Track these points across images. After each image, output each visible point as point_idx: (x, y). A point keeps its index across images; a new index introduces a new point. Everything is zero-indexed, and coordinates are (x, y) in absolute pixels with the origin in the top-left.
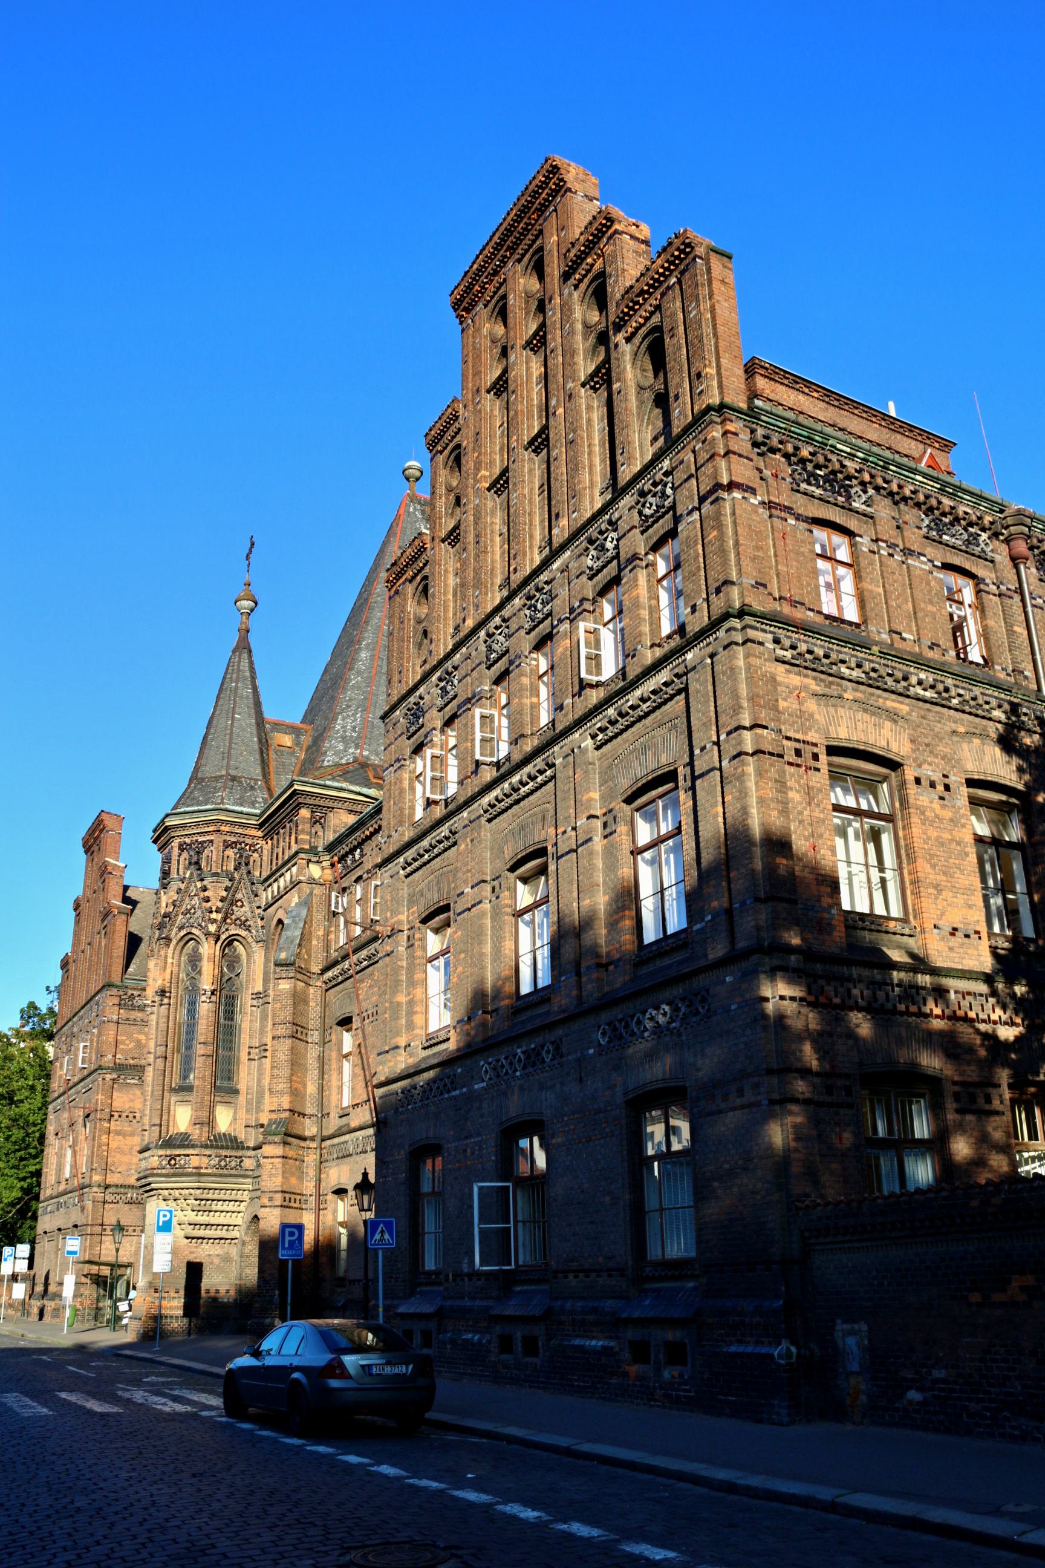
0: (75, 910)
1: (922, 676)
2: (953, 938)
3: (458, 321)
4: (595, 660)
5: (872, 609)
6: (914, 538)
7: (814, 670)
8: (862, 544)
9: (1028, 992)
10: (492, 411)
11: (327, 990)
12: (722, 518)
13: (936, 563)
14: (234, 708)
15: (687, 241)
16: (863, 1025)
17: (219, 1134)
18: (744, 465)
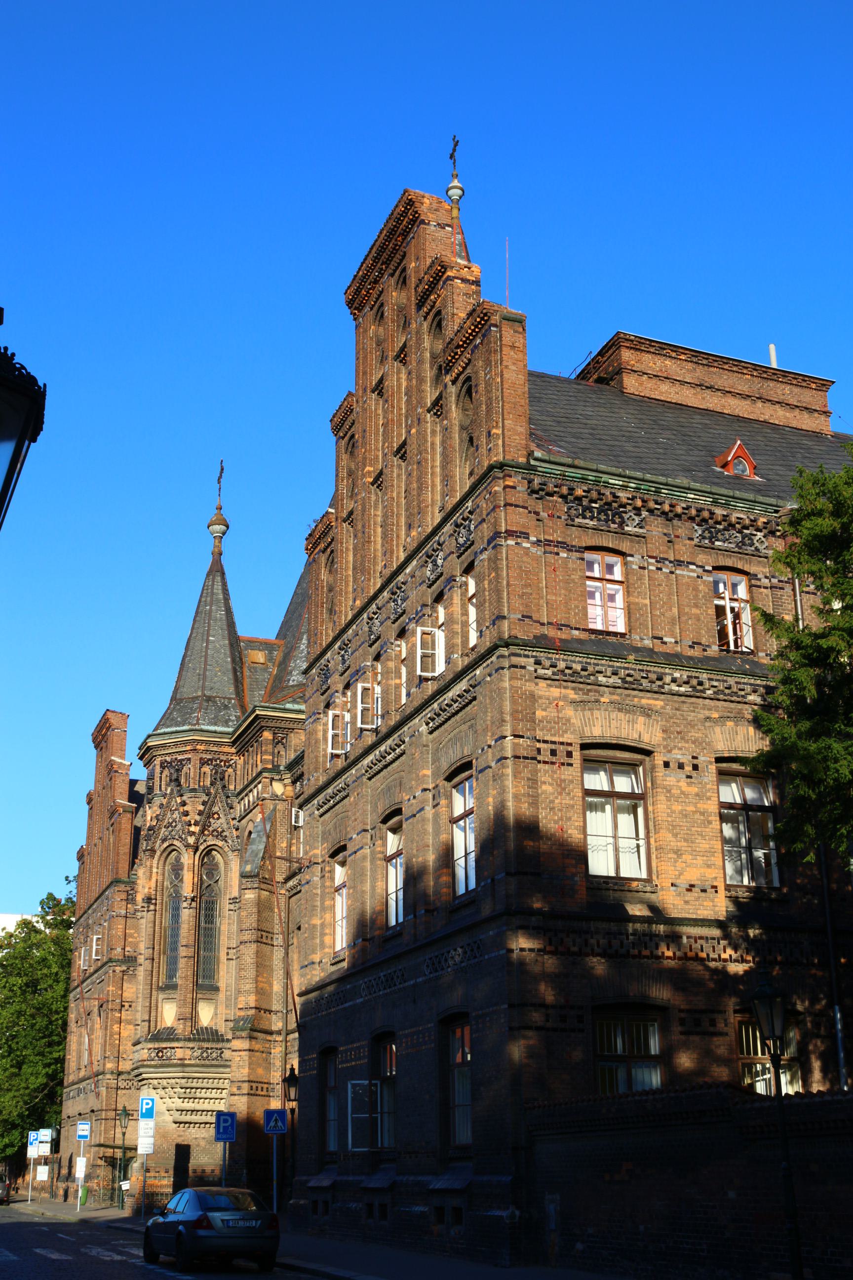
0: (88, 803)
1: (677, 675)
2: (689, 894)
3: (352, 317)
5: (637, 619)
6: (683, 550)
7: (573, 682)
8: (632, 562)
9: (761, 934)
10: (376, 410)
11: (290, 898)
12: (498, 562)
13: (707, 568)
15: (485, 311)
16: (599, 966)
17: (202, 1028)
18: (520, 514)
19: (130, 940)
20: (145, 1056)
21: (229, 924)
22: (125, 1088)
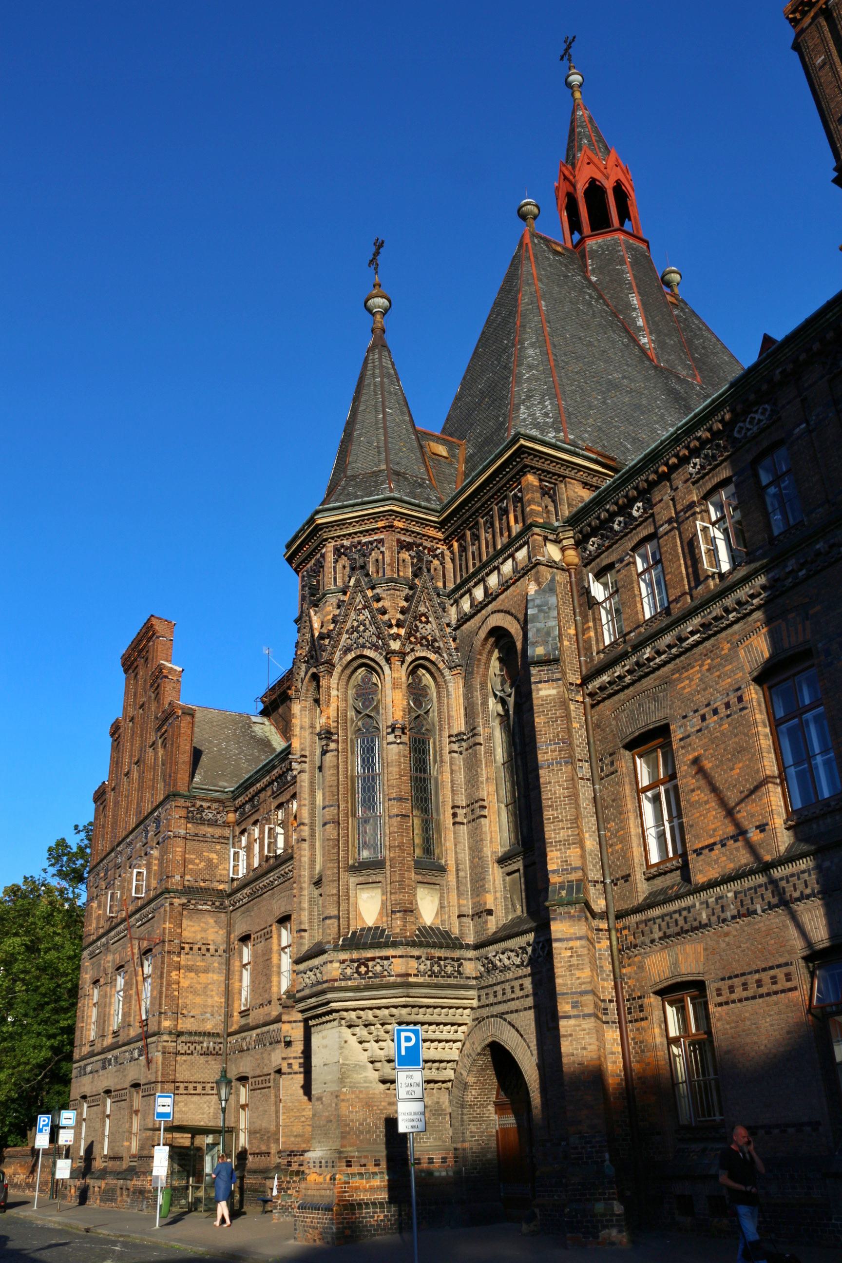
0: (112, 735)
11: (593, 706)
14: (383, 402)
17: (424, 927)
19: (190, 866)
22: (185, 1054)
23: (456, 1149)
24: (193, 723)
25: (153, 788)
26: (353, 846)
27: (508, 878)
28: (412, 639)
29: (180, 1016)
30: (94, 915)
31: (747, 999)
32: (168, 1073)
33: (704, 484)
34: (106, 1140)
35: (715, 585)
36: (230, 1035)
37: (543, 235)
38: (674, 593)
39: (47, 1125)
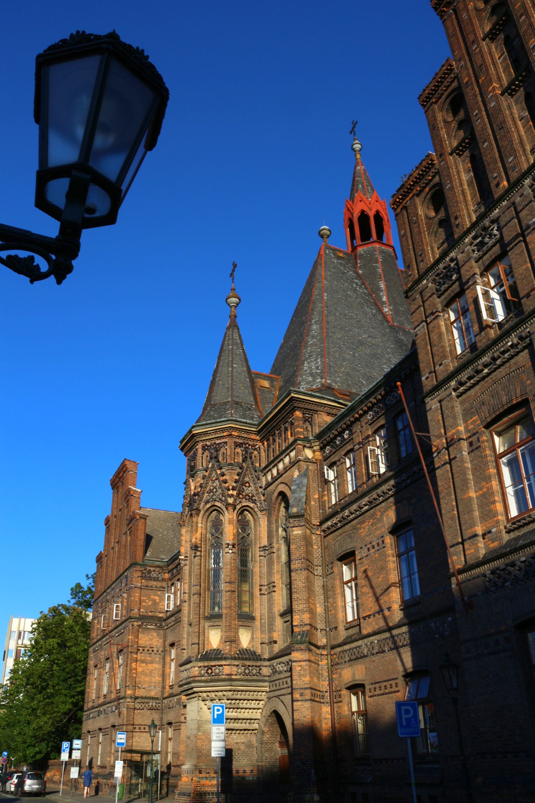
0: (106, 524)
4: (491, 310)
11: (325, 537)
14: (232, 360)
17: (242, 649)
19: (144, 604)
20: (196, 673)
21: (260, 566)
22: (139, 709)
23: (258, 766)
24: (145, 523)
25: (125, 558)
26: (208, 606)
27: (285, 624)
28: (241, 496)
29: (137, 688)
30: (96, 628)
31: (381, 695)
32: (130, 720)
33: (374, 426)
34: (99, 757)
35: (377, 481)
36: (164, 698)
37: (333, 246)
38: (360, 482)
39: (67, 748)
